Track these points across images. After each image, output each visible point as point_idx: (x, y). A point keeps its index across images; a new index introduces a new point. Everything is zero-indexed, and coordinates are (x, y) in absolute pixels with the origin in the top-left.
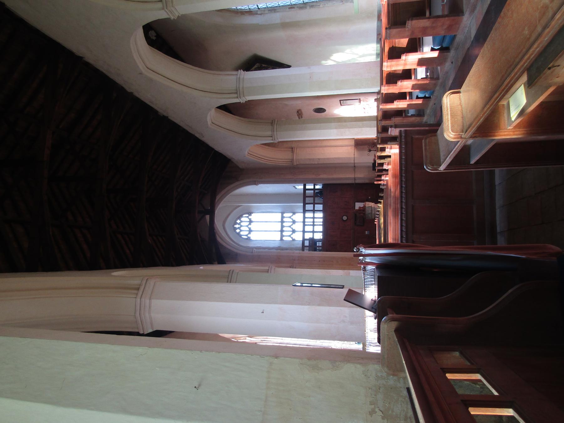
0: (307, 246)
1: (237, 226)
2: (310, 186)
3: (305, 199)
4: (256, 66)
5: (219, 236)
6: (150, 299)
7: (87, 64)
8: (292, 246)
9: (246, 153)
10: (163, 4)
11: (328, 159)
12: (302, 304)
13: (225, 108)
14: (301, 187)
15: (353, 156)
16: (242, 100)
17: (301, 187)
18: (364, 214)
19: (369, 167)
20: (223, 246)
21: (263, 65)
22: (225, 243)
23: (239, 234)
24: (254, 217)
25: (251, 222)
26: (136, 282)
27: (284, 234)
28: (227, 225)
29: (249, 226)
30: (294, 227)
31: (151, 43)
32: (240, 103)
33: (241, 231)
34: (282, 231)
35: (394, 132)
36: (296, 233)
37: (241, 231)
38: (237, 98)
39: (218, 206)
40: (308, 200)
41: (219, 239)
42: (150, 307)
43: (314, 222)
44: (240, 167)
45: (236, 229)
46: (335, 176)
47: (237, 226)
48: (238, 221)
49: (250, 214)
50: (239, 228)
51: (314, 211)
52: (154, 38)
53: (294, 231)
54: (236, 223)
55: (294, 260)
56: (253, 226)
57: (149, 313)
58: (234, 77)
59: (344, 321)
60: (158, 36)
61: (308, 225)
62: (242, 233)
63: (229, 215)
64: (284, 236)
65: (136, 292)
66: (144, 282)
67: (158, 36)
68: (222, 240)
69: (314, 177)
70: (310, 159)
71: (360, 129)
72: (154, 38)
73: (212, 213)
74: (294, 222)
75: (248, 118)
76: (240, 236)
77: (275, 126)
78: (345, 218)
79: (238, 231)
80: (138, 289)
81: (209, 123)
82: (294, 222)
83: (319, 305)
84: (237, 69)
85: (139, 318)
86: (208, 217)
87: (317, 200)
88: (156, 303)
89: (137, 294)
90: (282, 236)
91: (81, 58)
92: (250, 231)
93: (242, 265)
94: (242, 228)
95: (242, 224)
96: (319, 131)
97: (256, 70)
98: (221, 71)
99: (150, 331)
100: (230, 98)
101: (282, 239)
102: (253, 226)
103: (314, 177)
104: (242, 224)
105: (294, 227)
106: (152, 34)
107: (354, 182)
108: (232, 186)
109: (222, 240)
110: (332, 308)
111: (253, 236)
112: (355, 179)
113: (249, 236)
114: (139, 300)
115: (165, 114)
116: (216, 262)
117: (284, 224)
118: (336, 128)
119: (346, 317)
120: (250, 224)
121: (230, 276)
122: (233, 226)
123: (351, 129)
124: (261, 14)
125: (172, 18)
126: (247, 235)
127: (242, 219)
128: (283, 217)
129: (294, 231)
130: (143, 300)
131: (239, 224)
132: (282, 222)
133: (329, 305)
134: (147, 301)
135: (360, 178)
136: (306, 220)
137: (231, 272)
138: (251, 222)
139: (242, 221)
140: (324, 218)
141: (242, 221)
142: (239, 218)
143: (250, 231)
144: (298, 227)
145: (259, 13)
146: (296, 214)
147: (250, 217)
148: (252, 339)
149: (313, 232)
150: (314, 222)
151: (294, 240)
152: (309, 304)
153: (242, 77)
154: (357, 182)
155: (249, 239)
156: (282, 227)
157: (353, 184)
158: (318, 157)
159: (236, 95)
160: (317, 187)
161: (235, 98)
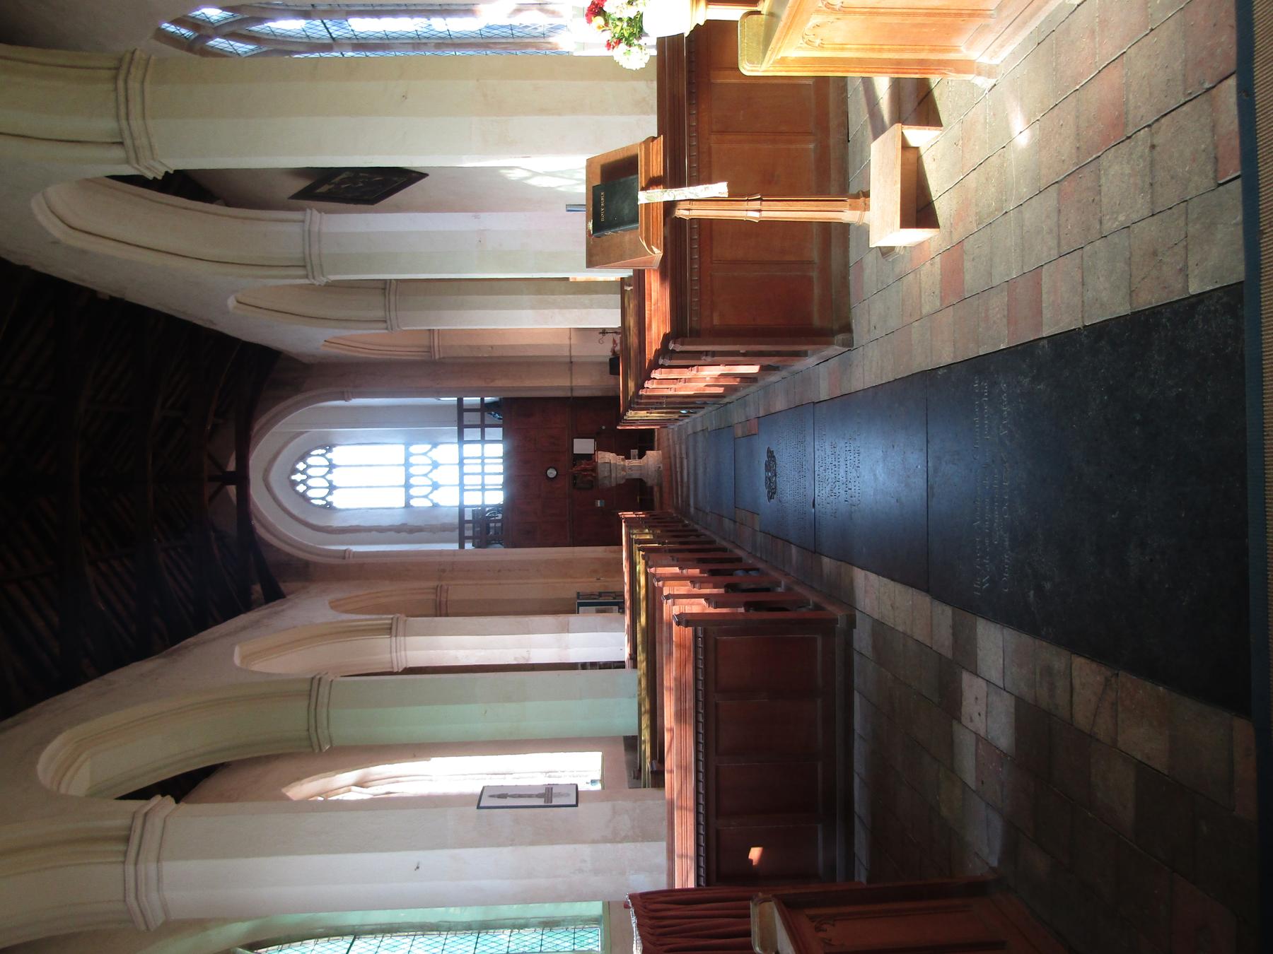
0: (469, 522)
1: (298, 477)
2: (468, 400)
3: (461, 419)
5: (259, 521)
6: (158, 860)
8: (434, 522)
10: (127, 152)
11: (513, 347)
12: (499, 845)
14: (453, 400)
15: (567, 342)
17: (453, 400)
18: (596, 478)
19: (601, 363)
20: (271, 546)
22: (272, 534)
23: (303, 496)
24: (338, 454)
25: (331, 466)
27: (413, 492)
28: (274, 478)
29: (329, 477)
30: (436, 476)
33: (309, 488)
34: (408, 486)
36: (440, 489)
37: (309, 488)
38: (307, 277)
40: (468, 418)
41: (261, 531)
42: (159, 880)
43: (483, 464)
45: (295, 483)
46: (528, 383)
47: (298, 477)
48: (301, 466)
49: (329, 447)
50: (303, 482)
51: (483, 440)
53: (435, 486)
54: (295, 471)
55: (444, 571)
56: (336, 477)
57: (159, 890)
58: (296, 228)
59: (581, 870)
61: (465, 473)
62: (310, 494)
64: (412, 497)
65: (122, 847)
68: (268, 530)
69: (481, 383)
70: (470, 346)
71: (584, 311)
73: (241, 478)
74: (435, 465)
76: (308, 500)
77: (392, 298)
78: (552, 473)
79: (301, 488)
80: (127, 840)
82: (435, 465)
83: (532, 843)
85: (135, 905)
86: (232, 490)
87: (489, 419)
88: (172, 868)
89: (125, 853)
90: (408, 498)
92: (332, 488)
94: (310, 482)
95: (310, 472)
96: (495, 312)
101: (407, 505)
102: (336, 477)
103: (481, 383)
104: (310, 472)
105: (436, 476)
107: (569, 395)
108: (290, 402)
109: (268, 530)
110: (558, 848)
111: (338, 500)
112: (572, 389)
113: (329, 499)
117: (412, 470)
118: (533, 308)
119: (585, 861)
120: (330, 472)
121: (314, 694)
122: (289, 477)
123: (564, 311)
126: (323, 499)
127: (310, 461)
128: (408, 455)
129: (435, 486)
130: (141, 866)
131: (303, 472)
132: (407, 465)
133: (552, 842)
134: (153, 867)
135: (584, 388)
136: (467, 480)
137: (316, 682)
138: (331, 466)
139: (309, 466)
140: (507, 456)
141: (309, 466)
142: (303, 458)
143: (332, 488)
144: (448, 475)
146: (440, 447)
147: (329, 455)
149: (483, 489)
150: (483, 464)
151: (435, 506)
152: (512, 842)
153: (315, 228)
154: (576, 394)
155: (329, 507)
156: (408, 476)
157: (568, 398)
158: (490, 343)
160: (487, 399)
161: (301, 277)
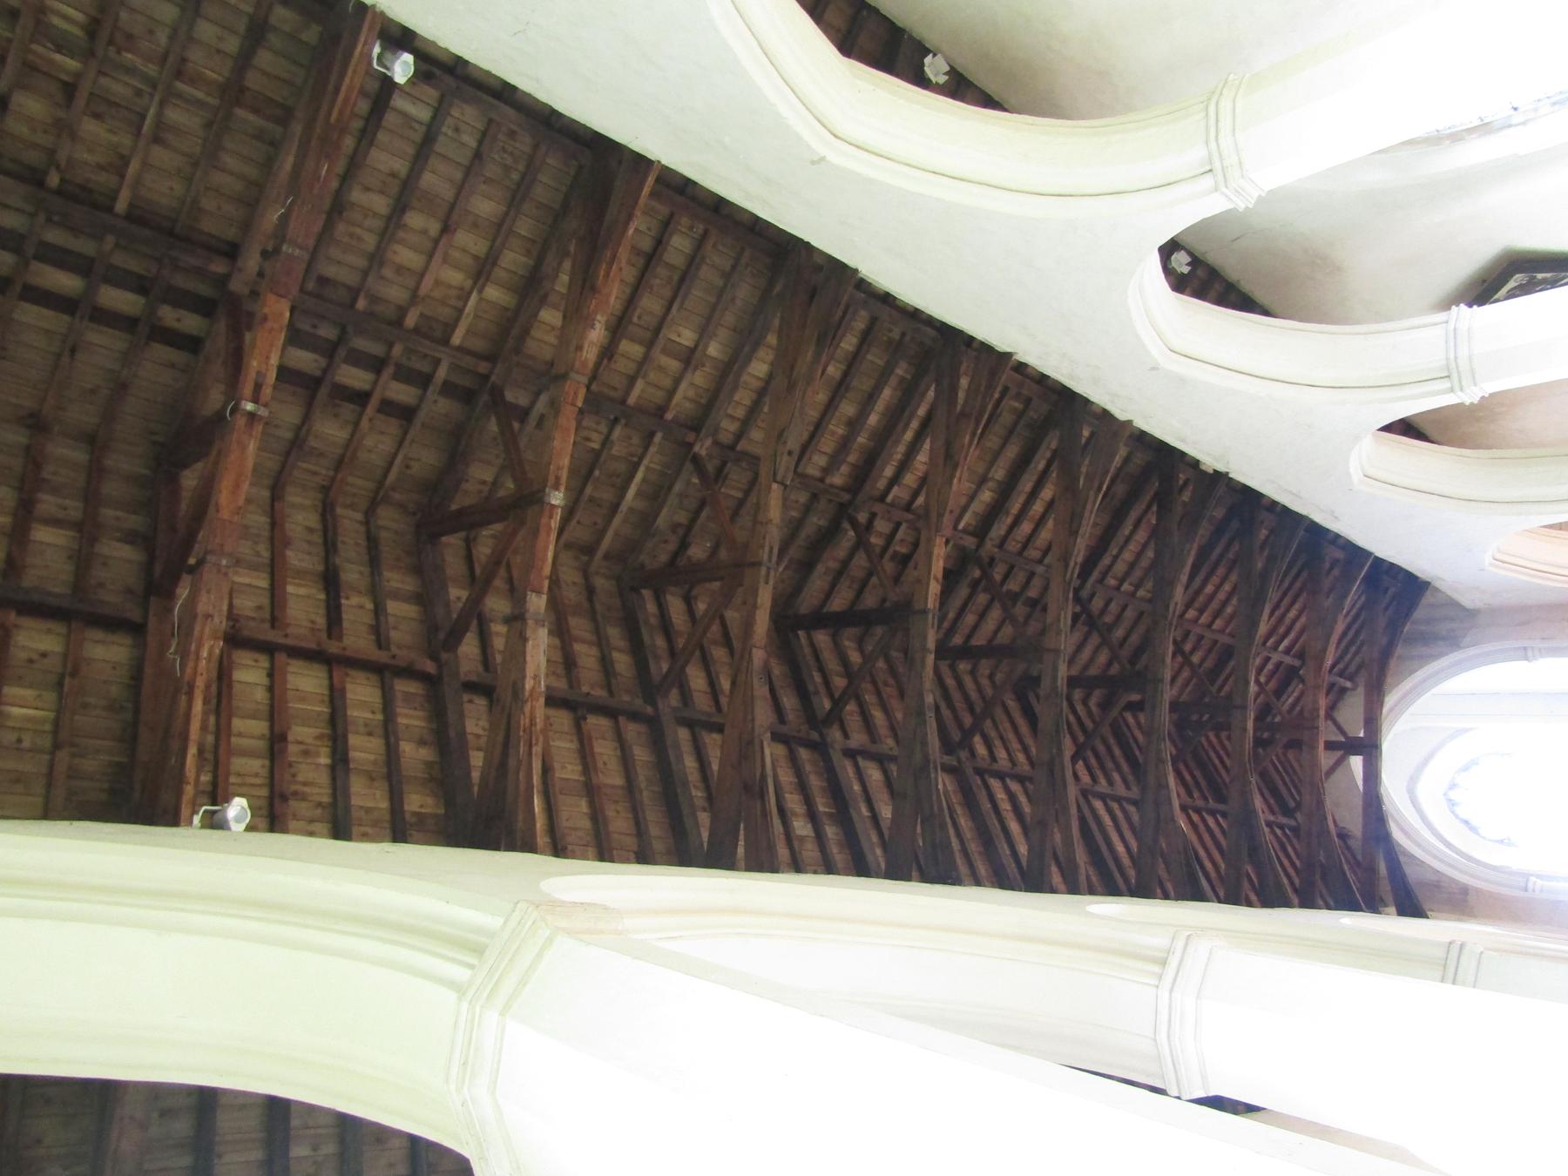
4: (1512, 284)
5: (1402, 830)
7: (1021, 367)
9: (1488, 559)
13: (1406, 428)
16: (1469, 396)
20: (1412, 857)
21: (1540, 276)
22: (1419, 846)
26: (1156, 941)
31: (1179, 283)
32: (1460, 406)
35: (723, 554)
38: (1452, 390)
39: (1392, 725)
41: (1397, 835)
44: (1466, 601)
52: (1186, 270)
60: (1196, 262)
63: (1431, 756)
65: (1157, 969)
66: (1180, 944)
67: (1196, 262)
72: (1186, 270)
75: (1489, 447)
80: (1163, 963)
81: (1356, 476)
84: (1448, 303)
89: (1160, 977)
91: (1007, 356)
93: (1490, 929)
97: (1511, 295)
98: (1389, 319)
99: (1201, 1094)
100: (1423, 395)
106: (1181, 262)
114: (1167, 995)
115: (1221, 468)
116: (1393, 909)
124: (1524, 123)
125: (1241, 206)
145: (1514, 121)
148: (200, 683)
159: (1446, 384)
